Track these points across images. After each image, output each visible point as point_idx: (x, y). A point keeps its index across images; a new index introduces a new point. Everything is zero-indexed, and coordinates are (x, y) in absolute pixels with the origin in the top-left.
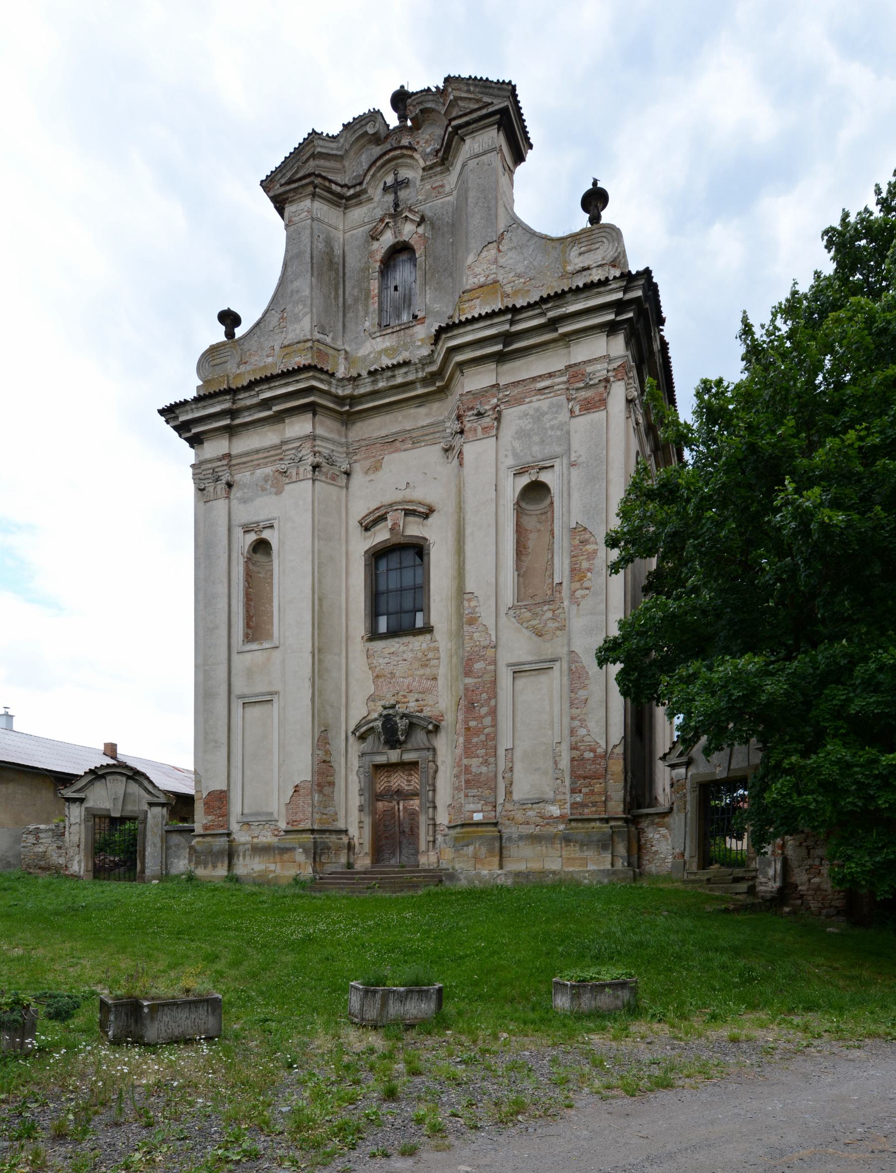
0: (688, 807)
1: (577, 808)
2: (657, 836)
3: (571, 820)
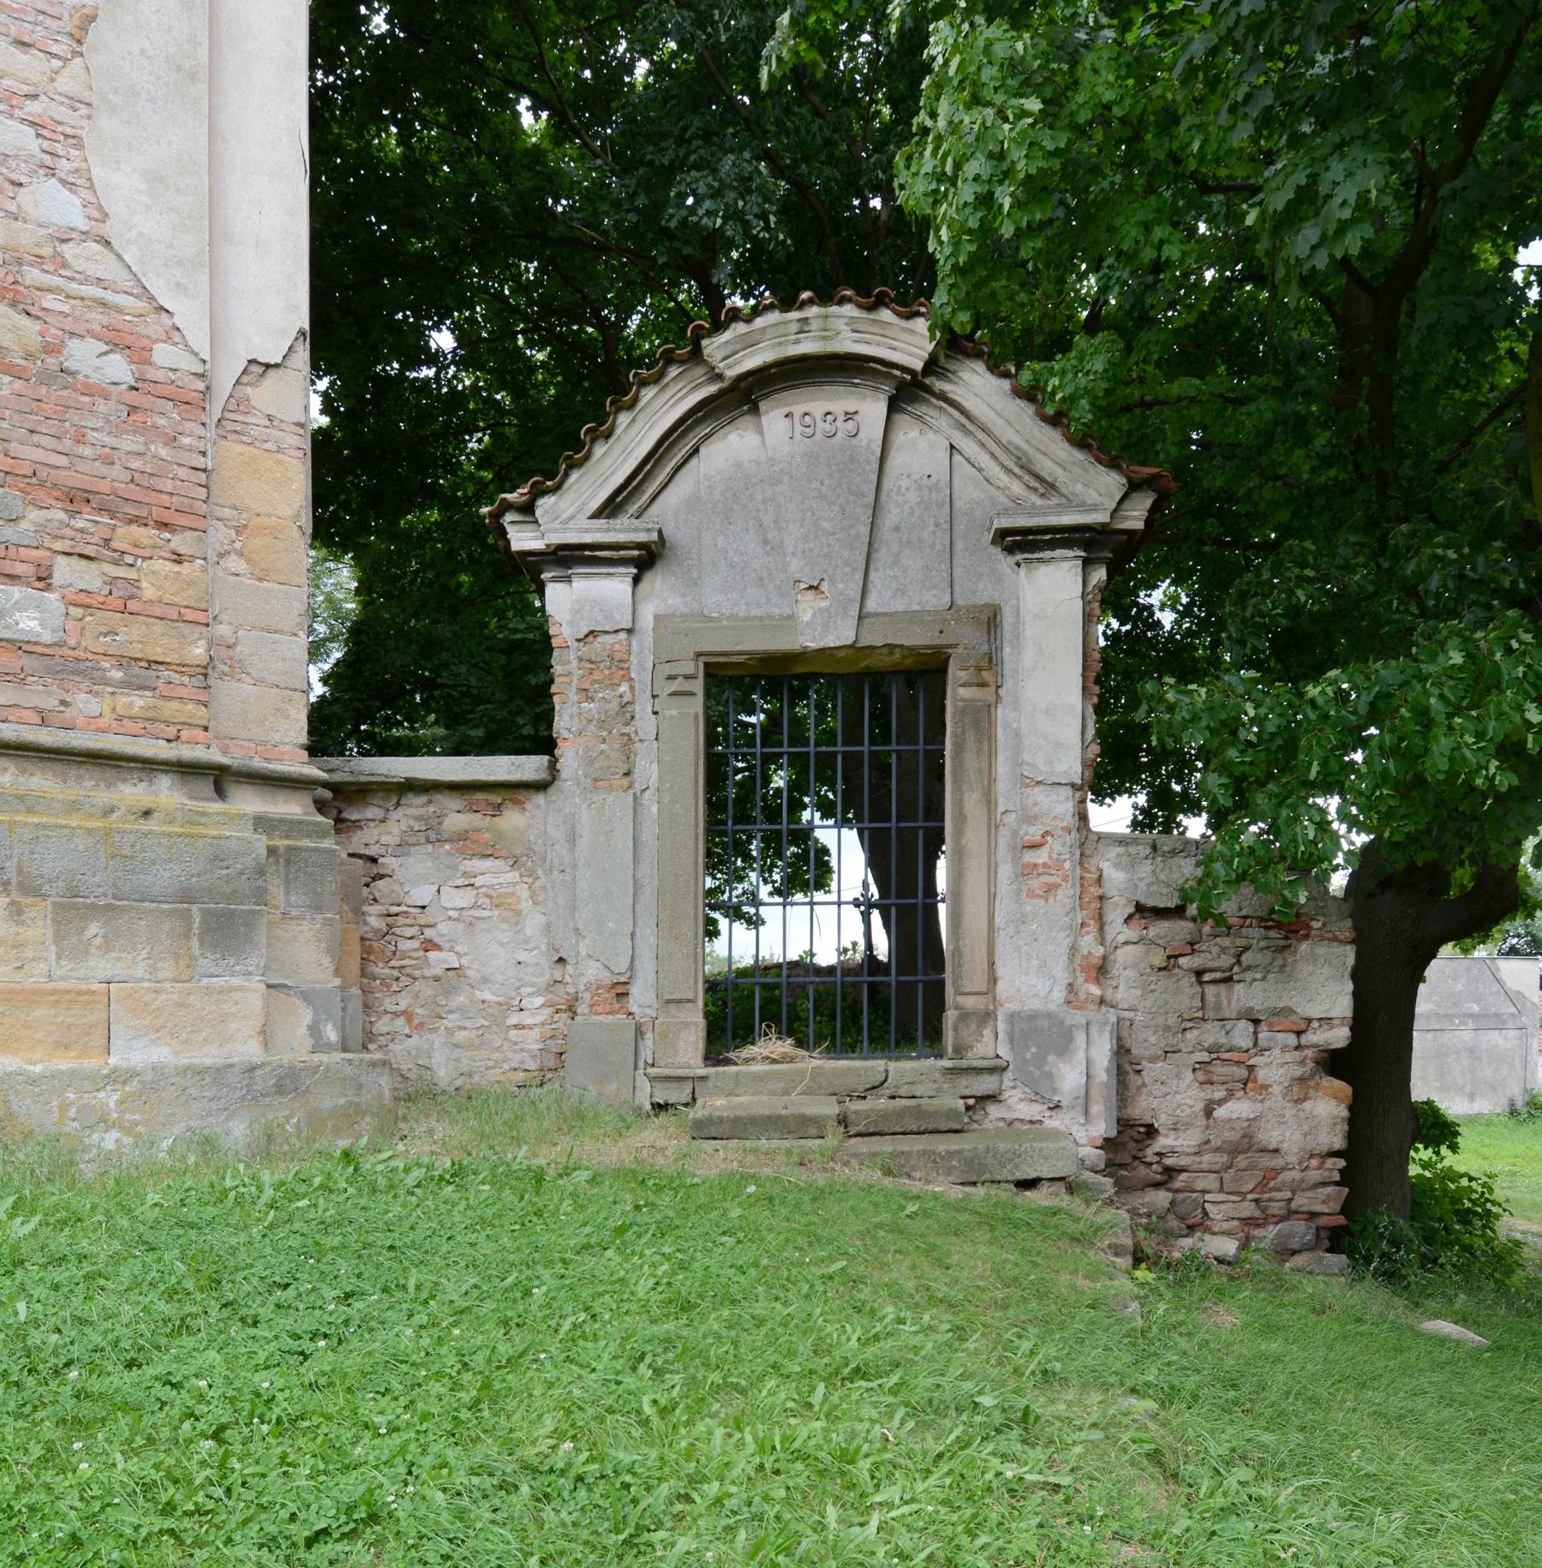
0: (648, 770)
2: (464, 899)
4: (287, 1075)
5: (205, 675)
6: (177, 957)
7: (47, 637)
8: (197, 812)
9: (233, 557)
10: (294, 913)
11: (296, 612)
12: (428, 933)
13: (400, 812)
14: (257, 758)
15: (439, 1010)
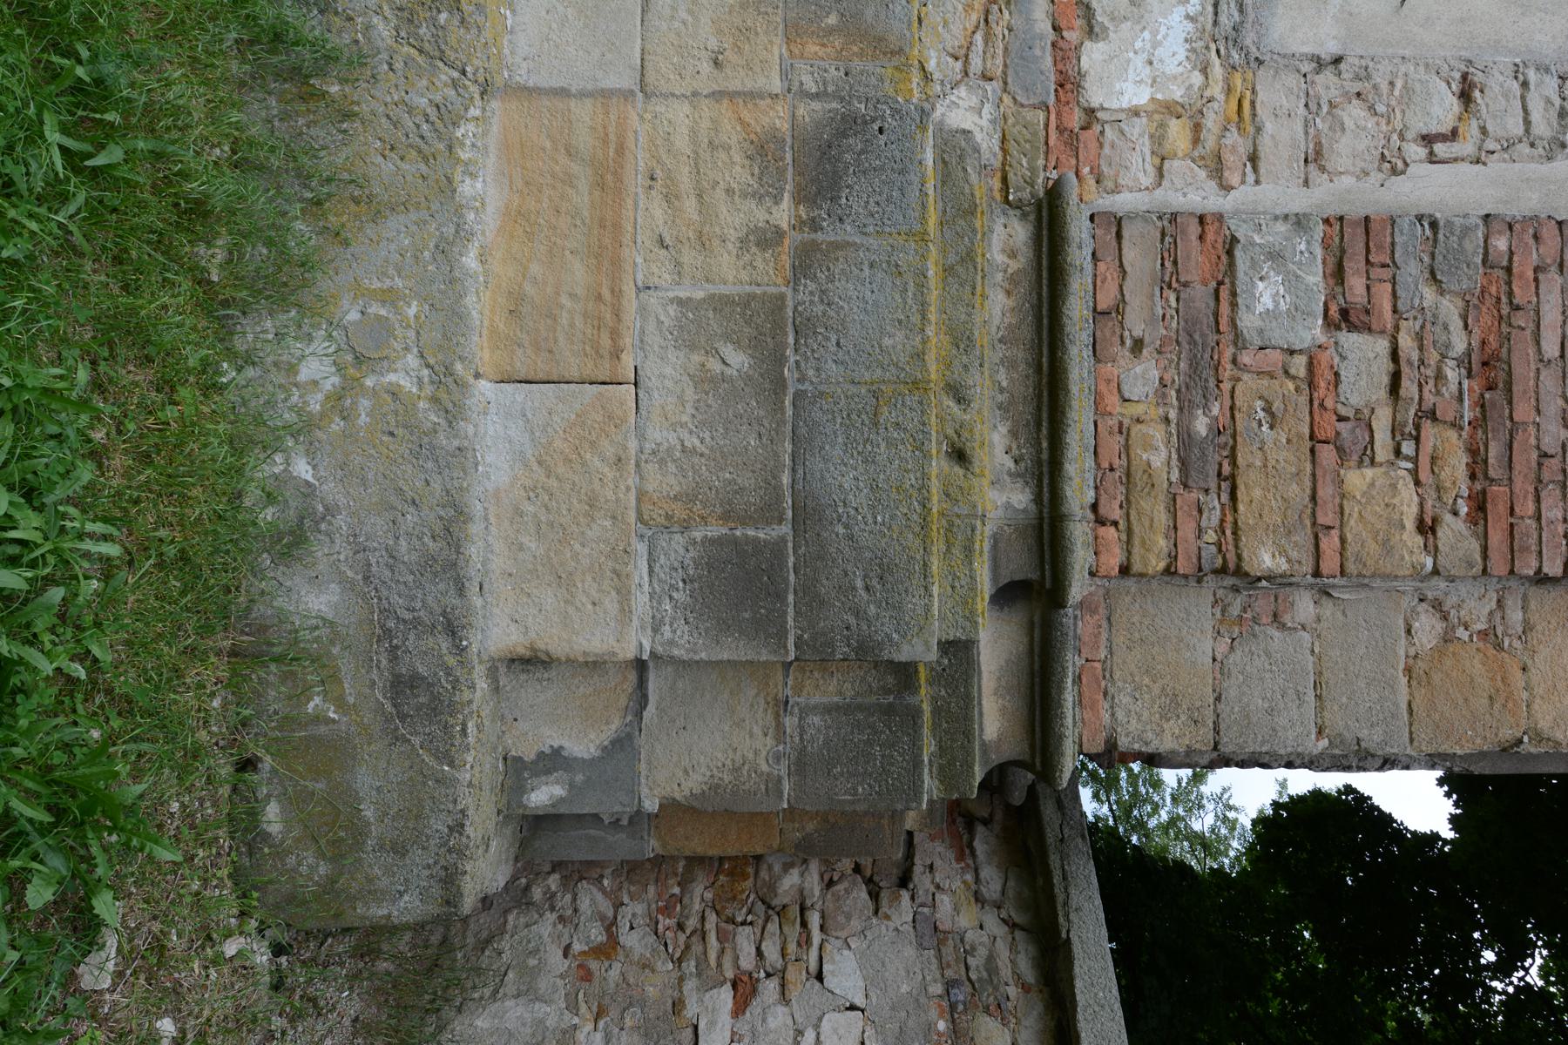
1: (1170, 279)
3: (1048, 217)
4: (435, 698)
5: (1222, 571)
6: (688, 498)
7: (1247, 322)
8: (971, 540)
9: (1440, 626)
10: (790, 722)
11: (1364, 734)
12: (770, 988)
13: (1000, 930)
14: (1079, 662)
15: (614, 1013)
